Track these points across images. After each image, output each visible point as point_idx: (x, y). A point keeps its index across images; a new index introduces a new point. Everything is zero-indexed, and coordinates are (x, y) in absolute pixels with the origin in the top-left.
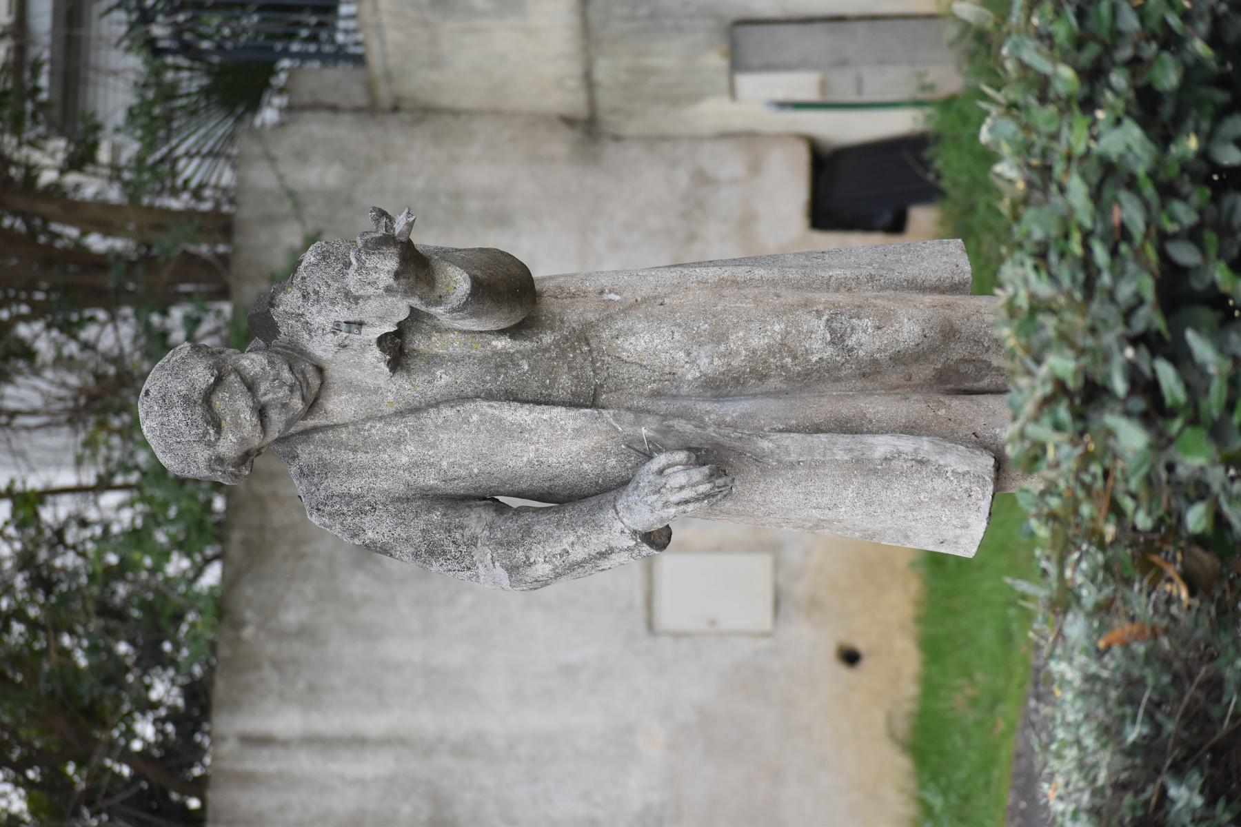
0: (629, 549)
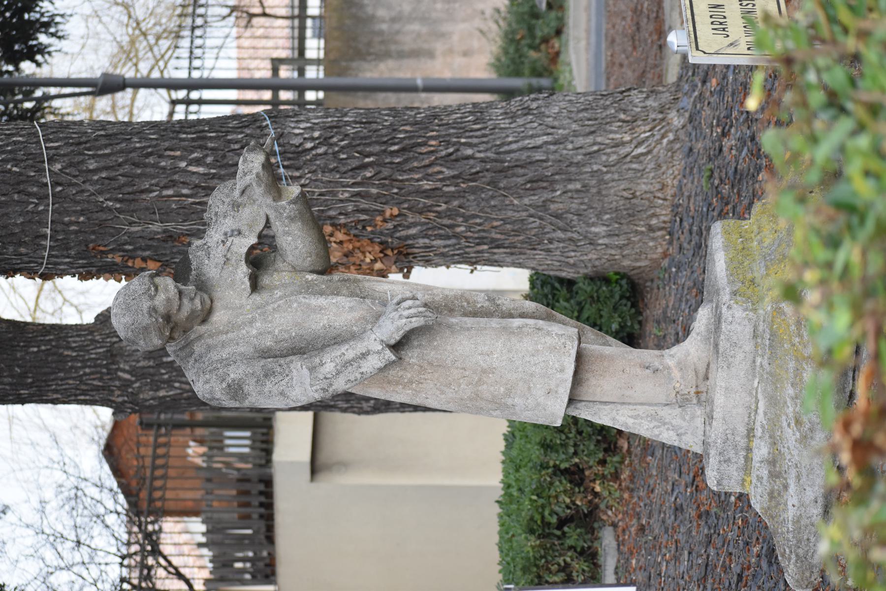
0: (378, 352)
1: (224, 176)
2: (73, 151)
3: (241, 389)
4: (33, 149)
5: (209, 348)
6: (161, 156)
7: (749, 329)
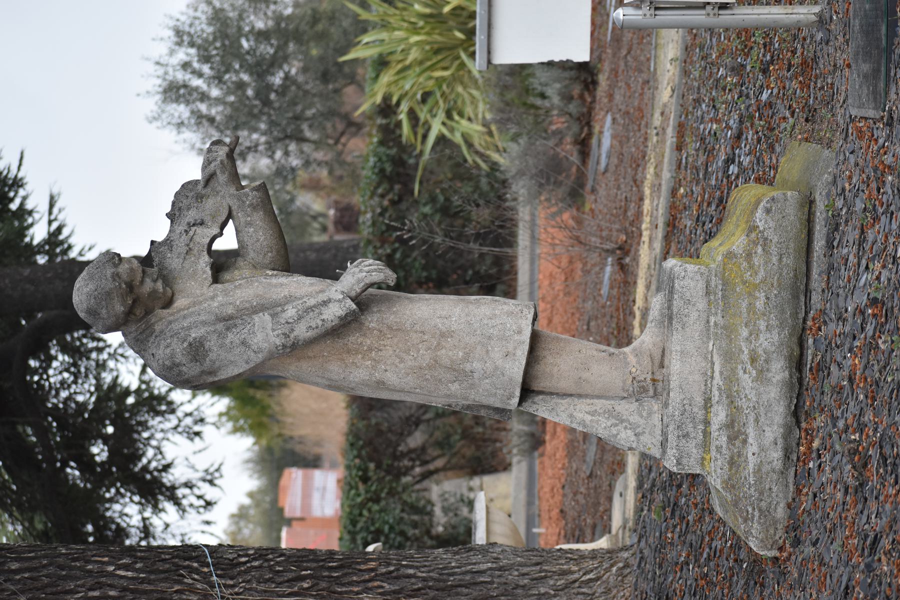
0: (339, 301)
1: (154, 581)
7: (701, 285)
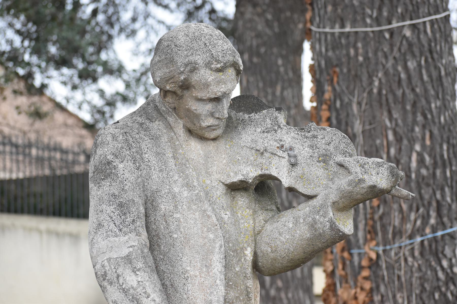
2: (423, 46)
3: (106, 177)
4: (424, 9)
5: (155, 139)
6: (424, 127)
